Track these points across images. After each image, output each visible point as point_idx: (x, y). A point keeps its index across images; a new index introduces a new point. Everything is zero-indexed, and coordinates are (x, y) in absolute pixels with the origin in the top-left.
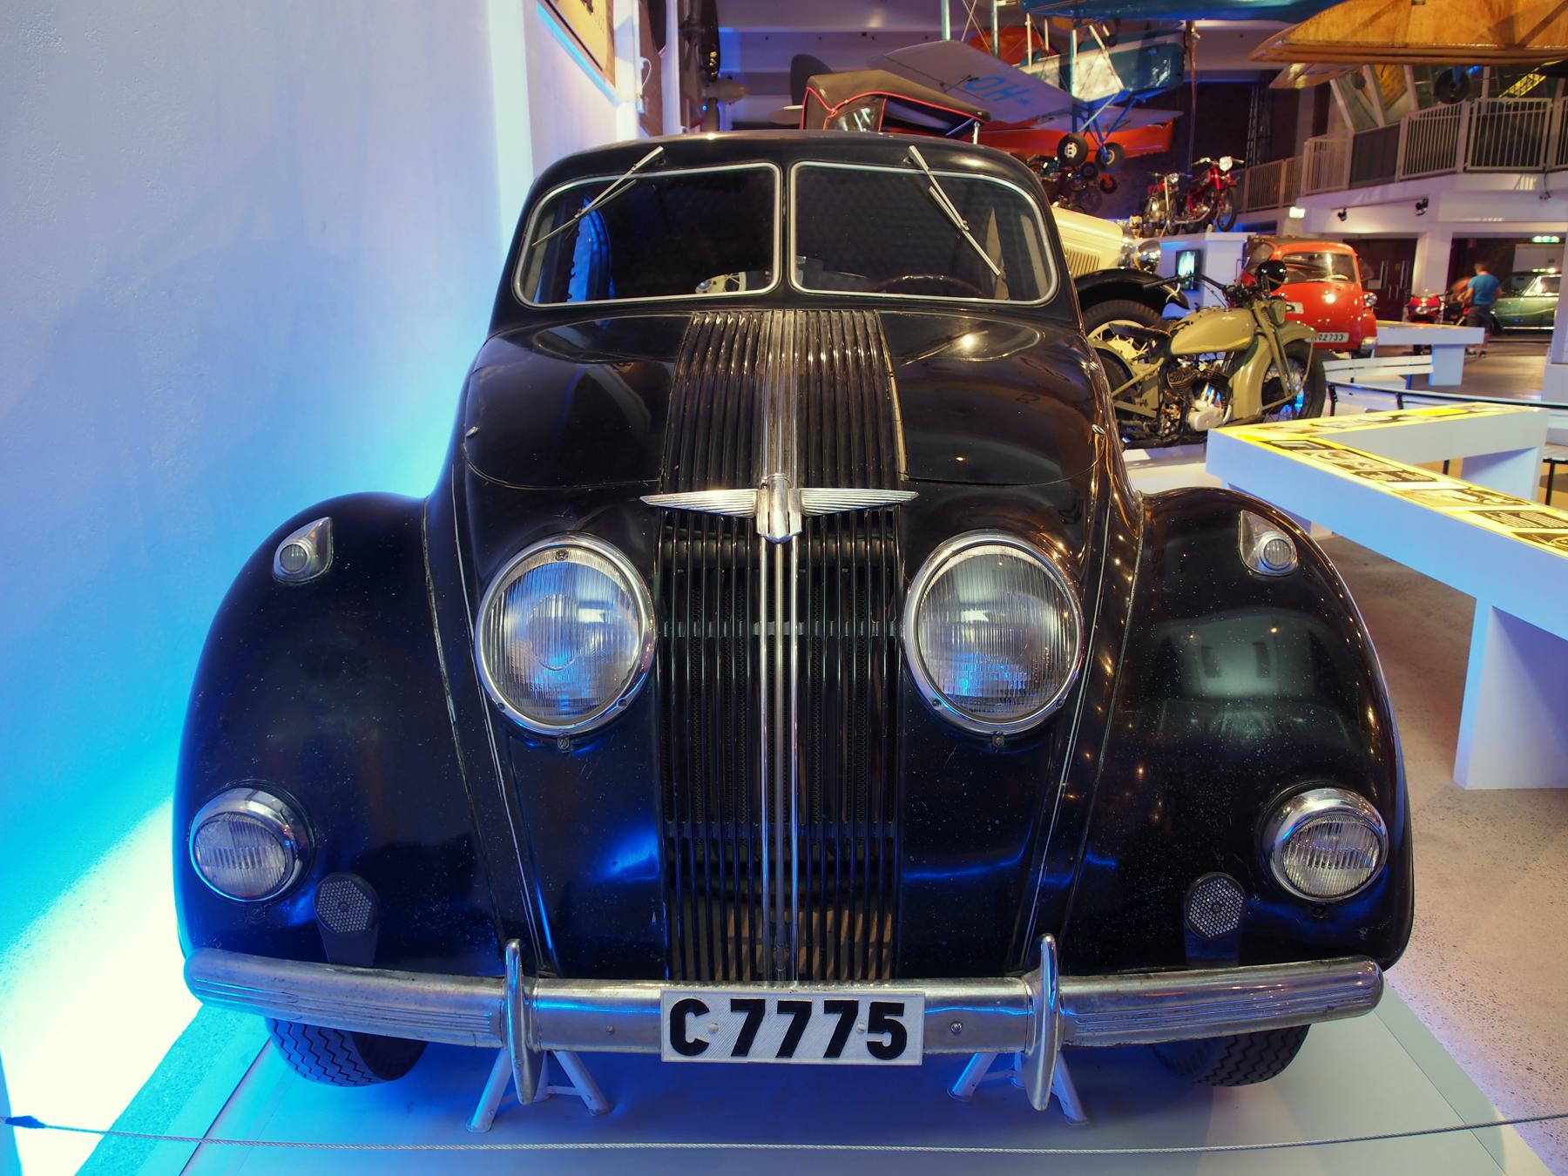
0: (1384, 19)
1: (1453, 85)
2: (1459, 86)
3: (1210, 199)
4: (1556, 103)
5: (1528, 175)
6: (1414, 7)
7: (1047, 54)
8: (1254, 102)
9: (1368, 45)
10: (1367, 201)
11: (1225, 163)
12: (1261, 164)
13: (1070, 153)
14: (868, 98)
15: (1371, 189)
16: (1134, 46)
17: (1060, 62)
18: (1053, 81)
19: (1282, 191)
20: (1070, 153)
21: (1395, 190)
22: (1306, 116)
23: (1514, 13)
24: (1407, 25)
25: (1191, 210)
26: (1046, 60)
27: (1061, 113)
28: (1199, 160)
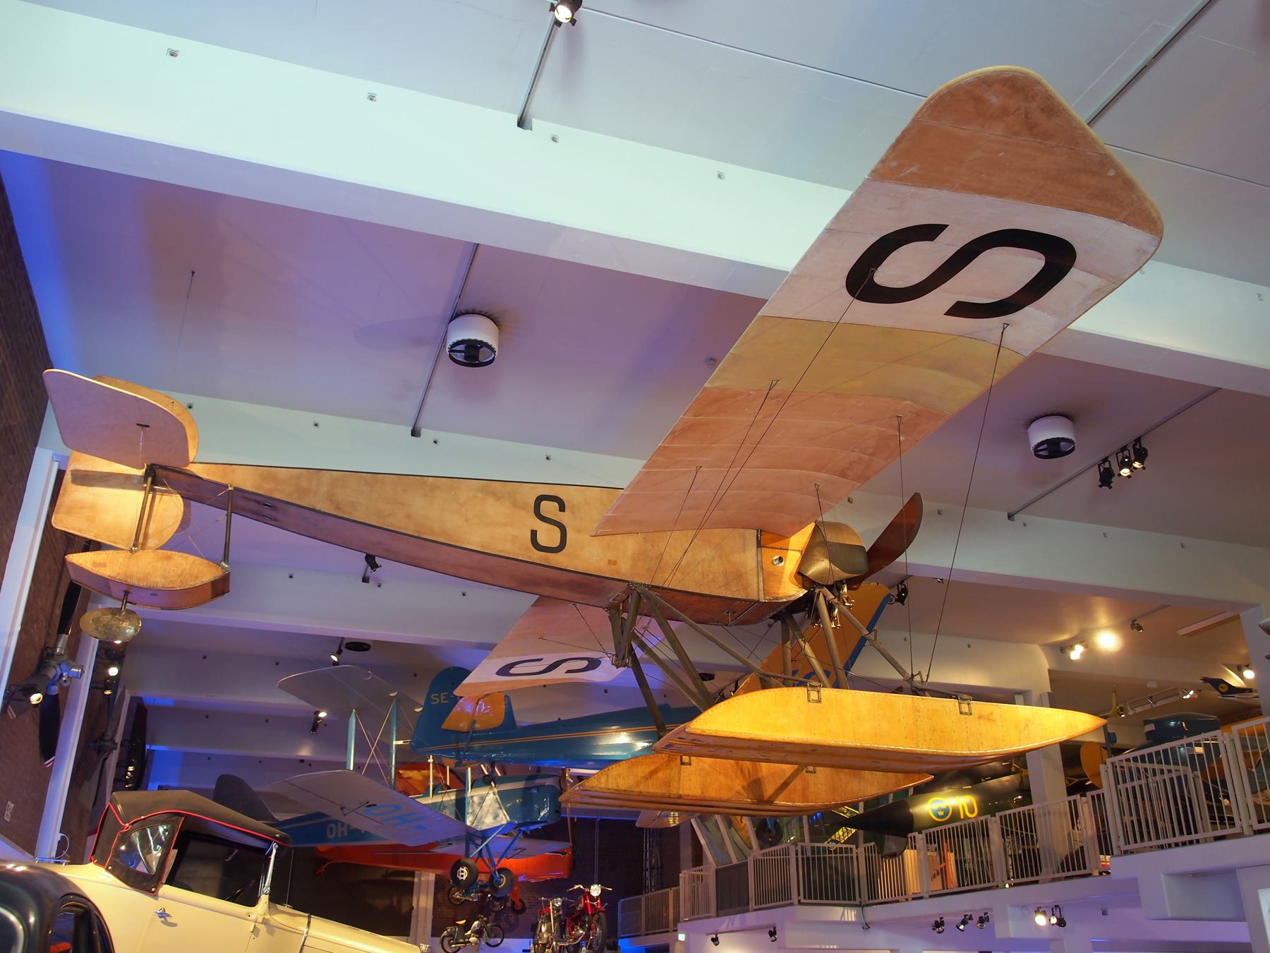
0: (660, 774)
1: (770, 831)
2: (774, 832)
3: (585, 922)
4: (859, 849)
5: (849, 908)
6: (683, 766)
7: (449, 788)
8: (646, 839)
9: (649, 795)
10: (731, 928)
11: (595, 890)
12: (655, 891)
13: (462, 876)
14: (165, 816)
15: (733, 916)
16: (520, 785)
17: (457, 795)
18: (449, 813)
19: (671, 917)
20: (462, 876)
21: (751, 918)
22: (686, 852)
23: (760, 776)
24: (679, 780)
25: (570, 933)
26: (445, 793)
27: (458, 839)
28: (573, 886)
